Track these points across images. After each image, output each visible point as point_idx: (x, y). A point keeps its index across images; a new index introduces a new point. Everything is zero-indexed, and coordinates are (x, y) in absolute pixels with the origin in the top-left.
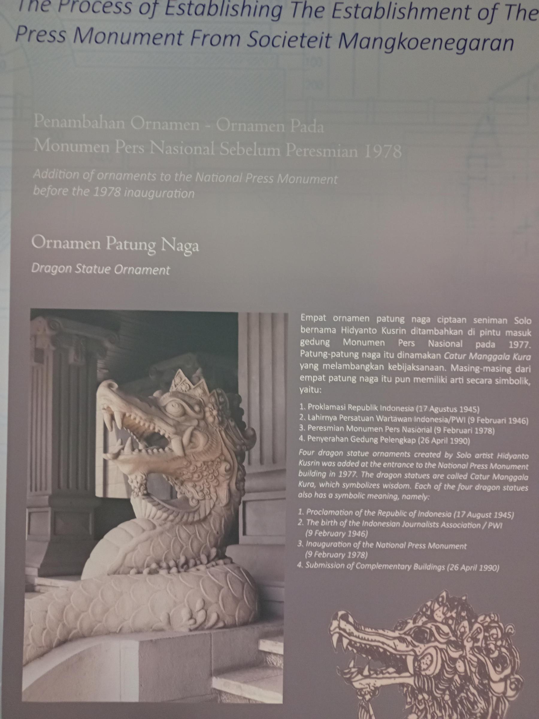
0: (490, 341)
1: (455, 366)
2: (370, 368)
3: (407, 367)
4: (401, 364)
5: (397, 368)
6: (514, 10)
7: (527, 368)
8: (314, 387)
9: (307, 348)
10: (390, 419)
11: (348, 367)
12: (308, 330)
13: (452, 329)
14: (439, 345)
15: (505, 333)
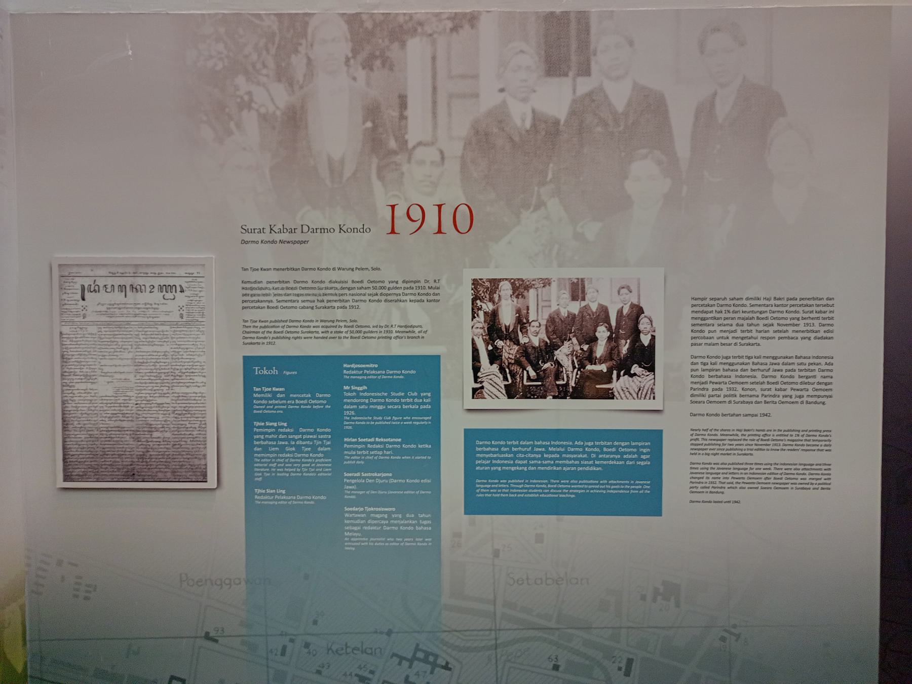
12: (480, 449)
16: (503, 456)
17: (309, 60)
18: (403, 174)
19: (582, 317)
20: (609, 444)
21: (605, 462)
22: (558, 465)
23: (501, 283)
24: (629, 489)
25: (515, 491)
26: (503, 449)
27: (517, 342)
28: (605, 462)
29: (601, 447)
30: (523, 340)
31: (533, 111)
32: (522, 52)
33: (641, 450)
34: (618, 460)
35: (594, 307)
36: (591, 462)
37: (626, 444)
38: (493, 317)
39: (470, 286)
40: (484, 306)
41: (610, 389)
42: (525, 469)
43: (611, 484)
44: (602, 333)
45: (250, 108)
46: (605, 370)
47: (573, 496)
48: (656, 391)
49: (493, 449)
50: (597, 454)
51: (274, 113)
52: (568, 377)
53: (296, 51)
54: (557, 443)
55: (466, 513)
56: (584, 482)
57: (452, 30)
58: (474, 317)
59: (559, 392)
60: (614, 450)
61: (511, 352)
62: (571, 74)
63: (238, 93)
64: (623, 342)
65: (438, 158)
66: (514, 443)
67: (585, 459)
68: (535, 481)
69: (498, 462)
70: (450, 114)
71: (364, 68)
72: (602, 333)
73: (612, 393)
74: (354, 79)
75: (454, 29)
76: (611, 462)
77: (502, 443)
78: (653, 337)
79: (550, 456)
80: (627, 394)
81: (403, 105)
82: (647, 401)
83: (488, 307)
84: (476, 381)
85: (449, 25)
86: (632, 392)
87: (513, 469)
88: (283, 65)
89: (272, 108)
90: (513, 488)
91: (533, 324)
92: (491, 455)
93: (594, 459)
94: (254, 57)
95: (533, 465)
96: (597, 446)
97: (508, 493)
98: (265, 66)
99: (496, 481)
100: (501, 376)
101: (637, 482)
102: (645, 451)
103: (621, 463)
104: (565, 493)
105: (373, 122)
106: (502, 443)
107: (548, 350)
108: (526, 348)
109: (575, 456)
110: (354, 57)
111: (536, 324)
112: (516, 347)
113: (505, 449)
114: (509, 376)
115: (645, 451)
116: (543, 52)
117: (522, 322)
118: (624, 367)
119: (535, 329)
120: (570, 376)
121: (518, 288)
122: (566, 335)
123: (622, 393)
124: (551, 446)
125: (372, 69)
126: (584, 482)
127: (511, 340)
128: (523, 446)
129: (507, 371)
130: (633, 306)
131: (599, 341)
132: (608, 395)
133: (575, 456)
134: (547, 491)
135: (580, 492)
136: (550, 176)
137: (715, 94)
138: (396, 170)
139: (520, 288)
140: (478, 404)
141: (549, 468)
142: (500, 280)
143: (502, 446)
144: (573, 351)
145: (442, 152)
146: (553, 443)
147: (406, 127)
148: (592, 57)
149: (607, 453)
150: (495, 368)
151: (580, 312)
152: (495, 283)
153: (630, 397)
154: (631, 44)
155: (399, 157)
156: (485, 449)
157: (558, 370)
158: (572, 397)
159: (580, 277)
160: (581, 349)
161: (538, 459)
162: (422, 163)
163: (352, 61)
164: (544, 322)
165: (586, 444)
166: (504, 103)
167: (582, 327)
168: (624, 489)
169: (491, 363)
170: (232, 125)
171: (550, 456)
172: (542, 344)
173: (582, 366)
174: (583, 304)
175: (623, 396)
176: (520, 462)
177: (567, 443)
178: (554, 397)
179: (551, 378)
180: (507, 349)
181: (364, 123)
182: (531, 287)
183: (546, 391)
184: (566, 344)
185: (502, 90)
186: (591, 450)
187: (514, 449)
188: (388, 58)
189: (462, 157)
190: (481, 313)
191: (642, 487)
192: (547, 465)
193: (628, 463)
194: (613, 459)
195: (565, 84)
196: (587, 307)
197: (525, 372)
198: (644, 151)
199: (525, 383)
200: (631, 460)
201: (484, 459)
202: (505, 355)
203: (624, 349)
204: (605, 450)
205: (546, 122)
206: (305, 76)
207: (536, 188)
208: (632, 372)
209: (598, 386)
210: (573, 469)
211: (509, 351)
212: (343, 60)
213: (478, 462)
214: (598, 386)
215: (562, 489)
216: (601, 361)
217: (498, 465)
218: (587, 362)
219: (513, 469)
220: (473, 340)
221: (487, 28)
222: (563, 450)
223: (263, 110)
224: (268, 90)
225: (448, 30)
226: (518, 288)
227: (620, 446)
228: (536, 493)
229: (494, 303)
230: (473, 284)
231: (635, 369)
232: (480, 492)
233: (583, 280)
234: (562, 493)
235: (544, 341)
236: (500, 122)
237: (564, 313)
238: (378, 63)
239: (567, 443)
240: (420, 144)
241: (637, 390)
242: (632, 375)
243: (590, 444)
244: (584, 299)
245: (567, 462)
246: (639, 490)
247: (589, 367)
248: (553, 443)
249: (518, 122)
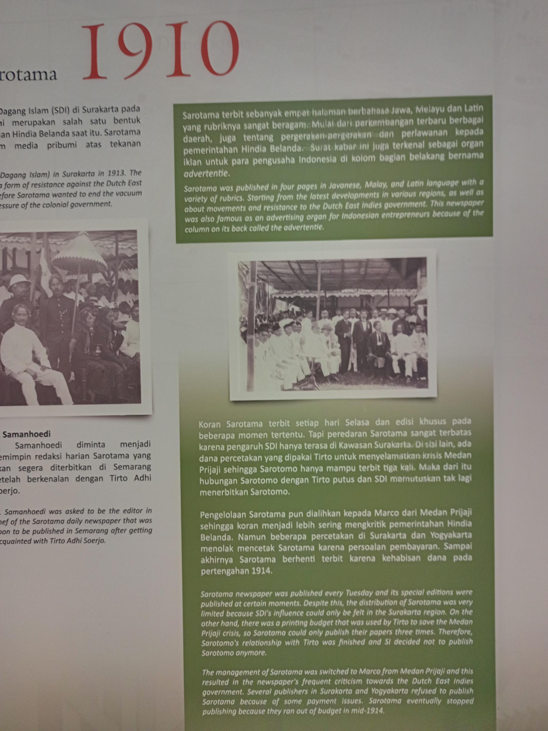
1: (378, 511)
2: (366, 526)
4: (236, 466)
6: (133, 172)
8: (218, 159)
9: (208, 698)
10: (464, 535)
13: (455, 532)
113: (419, 536)
213: (205, 644)
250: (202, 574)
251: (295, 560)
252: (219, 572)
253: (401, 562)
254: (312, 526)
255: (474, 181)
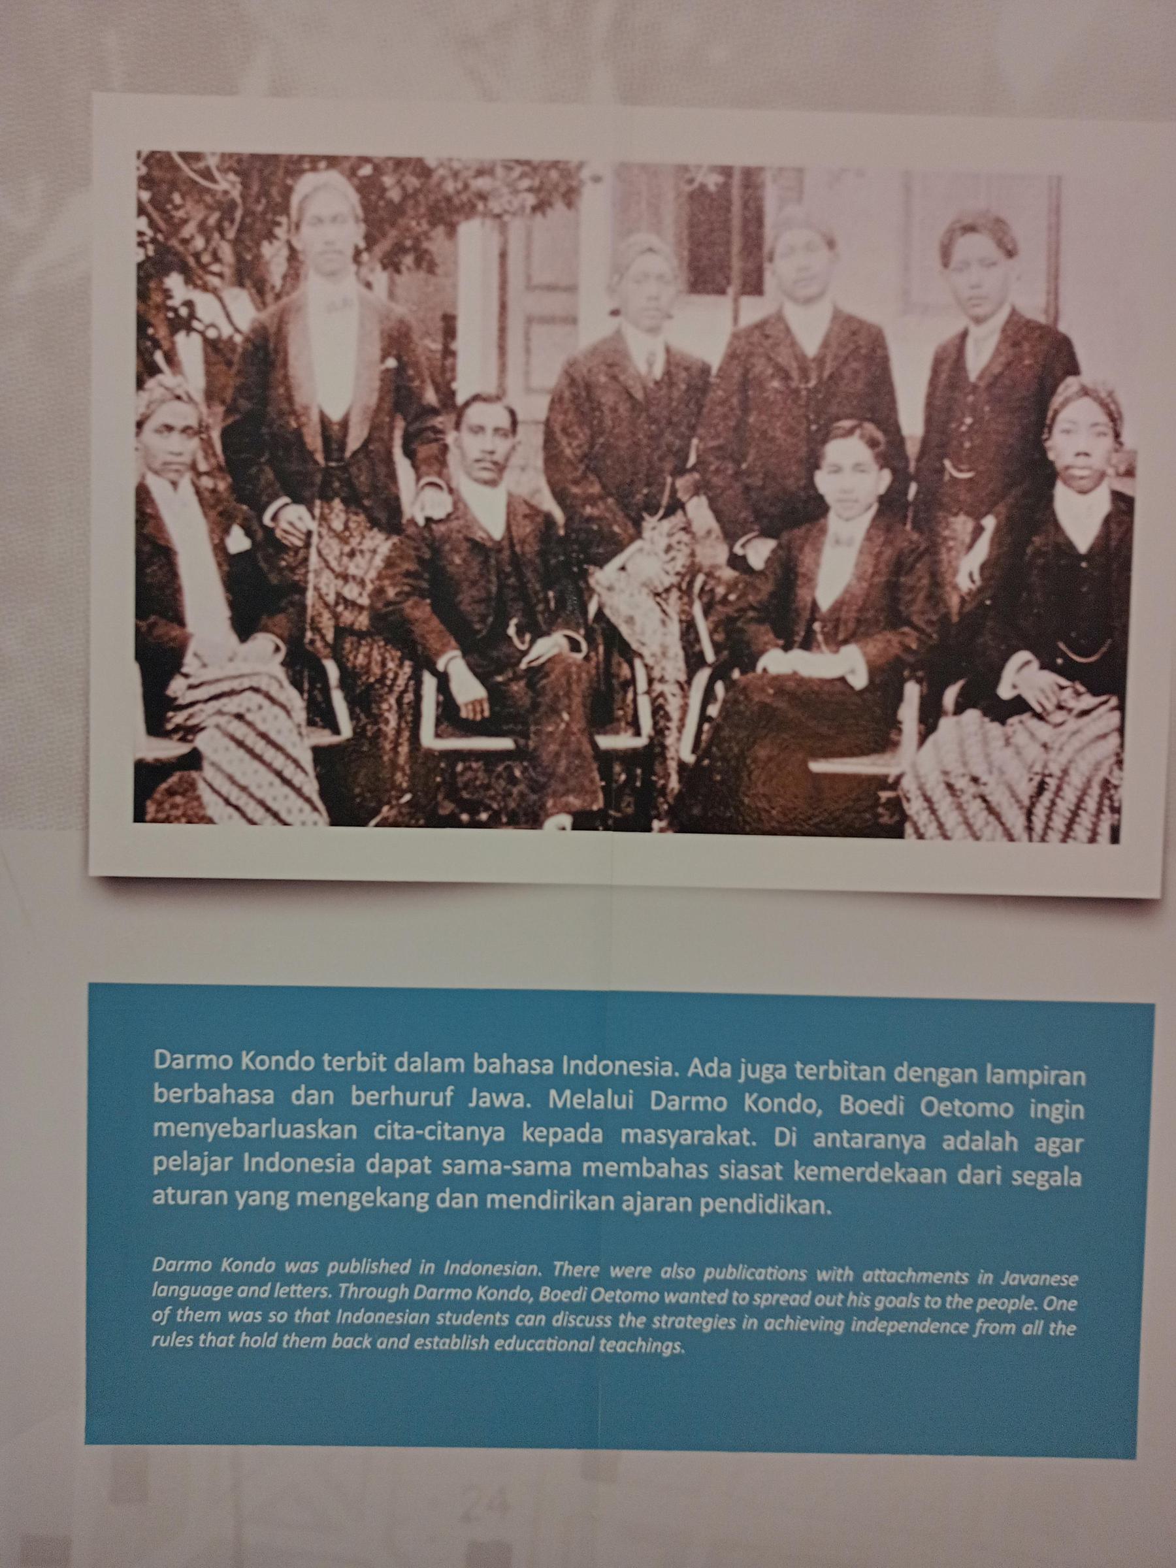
0: (519, 1288)
1: (560, 1096)
3: (210, 1162)
5: (231, 1132)
7: (990, 1173)
11: (634, 1169)
12: (173, 1095)
14: (750, 1173)
15: (152, 1129)
16: (300, 1132)
17: (293, 255)
18: (445, 448)
19: (745, 384)
20: (867, 1074)
21: (846, 1174)
22: (596, 1186)
23: (305, 184)
24: (969, 1316)
25: (361, 1317)
26: (299, 1096)
27: (387, 515)
28: (846, 1174)
29: (826, 1092)
30: (420, 502)
31: (668, 350)
32: (650, 250)
33: (1036, 1110)
34: (914, 1160)
35: (810, 332)
36: (772, 1172)
37: (960, 1076)
38: (254, 374)
39: (130, 193)
40: (207, 308)
41: (881, 782)
42: (421, 1203)
43: (876, 1290)
44: (850, 477)
45: (190, 329)
46: (859, 681)
47: (669, 1349)
48: (1126, 796)
49: (244, 1097)
50: (806, 1125)
51: (231, 338)
52: (658, 711)
53: (270, 236)
54: (594, 1067)
55: (92, 1438)
56: (730, 1273)
57: (535, 209)
58: (147, 370)
59: (612, 795)
60: (895, 1106)
61: (354, 568)
62: (731, 291)
63: (170, 303)
64: (962, 525)
65: (505, 422)
66: (363, 1063)
67: (741, 1155)
68: (469, 1269)
69: (276, 1164)
70: (528, 350)
71: (385, 267)
72: (850, 477)
73: (896, 805)
74: (369, 285)
75: (540, 207)
76: (877, 1174)
77: (297, 1062)
78: (1123, 505)
79: (553, 1136)
80: (975, 808)
81: (449, 329)
82: (1078, 847)
83: (231, 313)
84: (155, 726)
85: (531, 200)
86: (999, 797)
87: (354, 1201)
88: (249, 257)
89: (227, 331)
90: (354, 1305)
91: (474, 414)
92: (237, 1129)
93: (786, 1157)
94: (199, 243)
95: (460, 1184)
96: (807, 1088)
97: (326, 1330)
98: (216, 259)
99: (264, 1266)
100: (296, 701)
101: (1011, 1279)
102: (1056, 1114)
103: (928, 1176)
104: (631, 1334)
105: (399, 358)
106: (297, 1062)
107: (554, 566)
108: (435, 546)
109: (688, 1138)
110: (369, 249)
111: (495, 415)
112: (381, 544)
113: (315, 1098)
114: (338, 699)
115: (1056, 1114)
116: (686, 253)
117: (415, 400)
118: (957, 664)
119: (488, 441)
120: (673, 707)
121: (398, 210)
122: (653, 479)
123: (944, 804)
124: (560, 1081)
125: (398, 270)
126: (730, 1273)
127: (352, 501)
128: (410, 1082)
129: (332, 670)
130: (1019, 332)
131: (834, 522)
132: (875, 814)
133: (688, 1138)
134: (530, 1321)
135: (707, 1325)
136: (692, 460)
137: (964, 335)
138: (437, 440)
139: (406, 213)
140: (167, 848)
141: (548, 1201)
142: (296, 165)
143: (298, 1078)
144: (693, 570)
145: (512, 413)
146: (569, 1066)
147: (453, 369)
148: (767, 265)
149: (856, 1124)
150: (264, 655)
151: (732, 356)
152: (268, 180)
153: (991, 829)
154: (831, 244)
155: (440, 419)
156: (199, 1094)
157: (607, 673)
158: (683, 823)
159: (740, 159)
160: (737, 562)
161: (492, 1151)
162: (479, 430)
163: (365, 257)
164: (534, 409)
165: (747, 1071)
166: (618, 335)
167: (742, 445)
168: (942, 1315)
169: (244, 627)
170: (159, 357)
171: (553, 1136)
172: (525, 529)
173: (737, 653)
174: (753, 311)
175: (951, 819)
176: (395, 1167)
177: (650, 1069)
178: (583, 821)
179: (570, 719)
180: (333, 548)
181: (383, 359)
182: (469, 210)
183: (537, 787)
184: (656, 530)
185: (615, 313)
186: (770, 1105)
187: (359, 1097)
188: (426, 251)
189: (548, 423)
190: (189, 348)
191: (1034, 1303)
192: (536, 1185)
193: (967, 1176)
194: (888, 1157)
195: (723, 304)
196: (768, 334)
197: (429, 683)
198: (847, 424)
199: (428, 739)
200: (983, 1160)
201: (196, 1145)
202: (321, 584)
203: (968, 565)
204: (847, 1105)
205: (687, 369)
206: (285, 277)
207: (669, 480)
208: (1005, 692)
209: (818, 766)
210: (673, 1205)
211: (343, 564)
212: (350, 252)
213: (160, 1164)
214: (818, 766)
215: (615, 1309)
216: (841, 629)
217: (275, 1182)
218: (764, 634)
219: (354, 1201)
220: (143, 495)
221: (595, 202)
222: (626, 1103)
223: (212, 334)
224: (220, 299)
225: (528, 210)
226: (398, 210)
227: (930, 1087)
228: (474, 1331)
229: (260, 289)
230: (145, 182)
231: (1022, 675)
232: (173, 1326)
233: (751, 178)
234: (615, 1333)
235: (534, 512)
236: (610, 366)
237: (646, 359)
238: (408, 260)
239: (650, 1069)
240: (476, 398)
241: (1025, 790)
242: (1004, 711)
243: (767, 1073)
244: (754, 286)
245: (645, 1169)
246: (1020, 1317)
247: (776, 661)
248: (569, 1066)
249: (643, 368)
250: (157, 1168)
251: (388, 1098)
252: (324, 1199)
253: (450, 1351)
254: (1011, 1143)
255: (849, 1273)
